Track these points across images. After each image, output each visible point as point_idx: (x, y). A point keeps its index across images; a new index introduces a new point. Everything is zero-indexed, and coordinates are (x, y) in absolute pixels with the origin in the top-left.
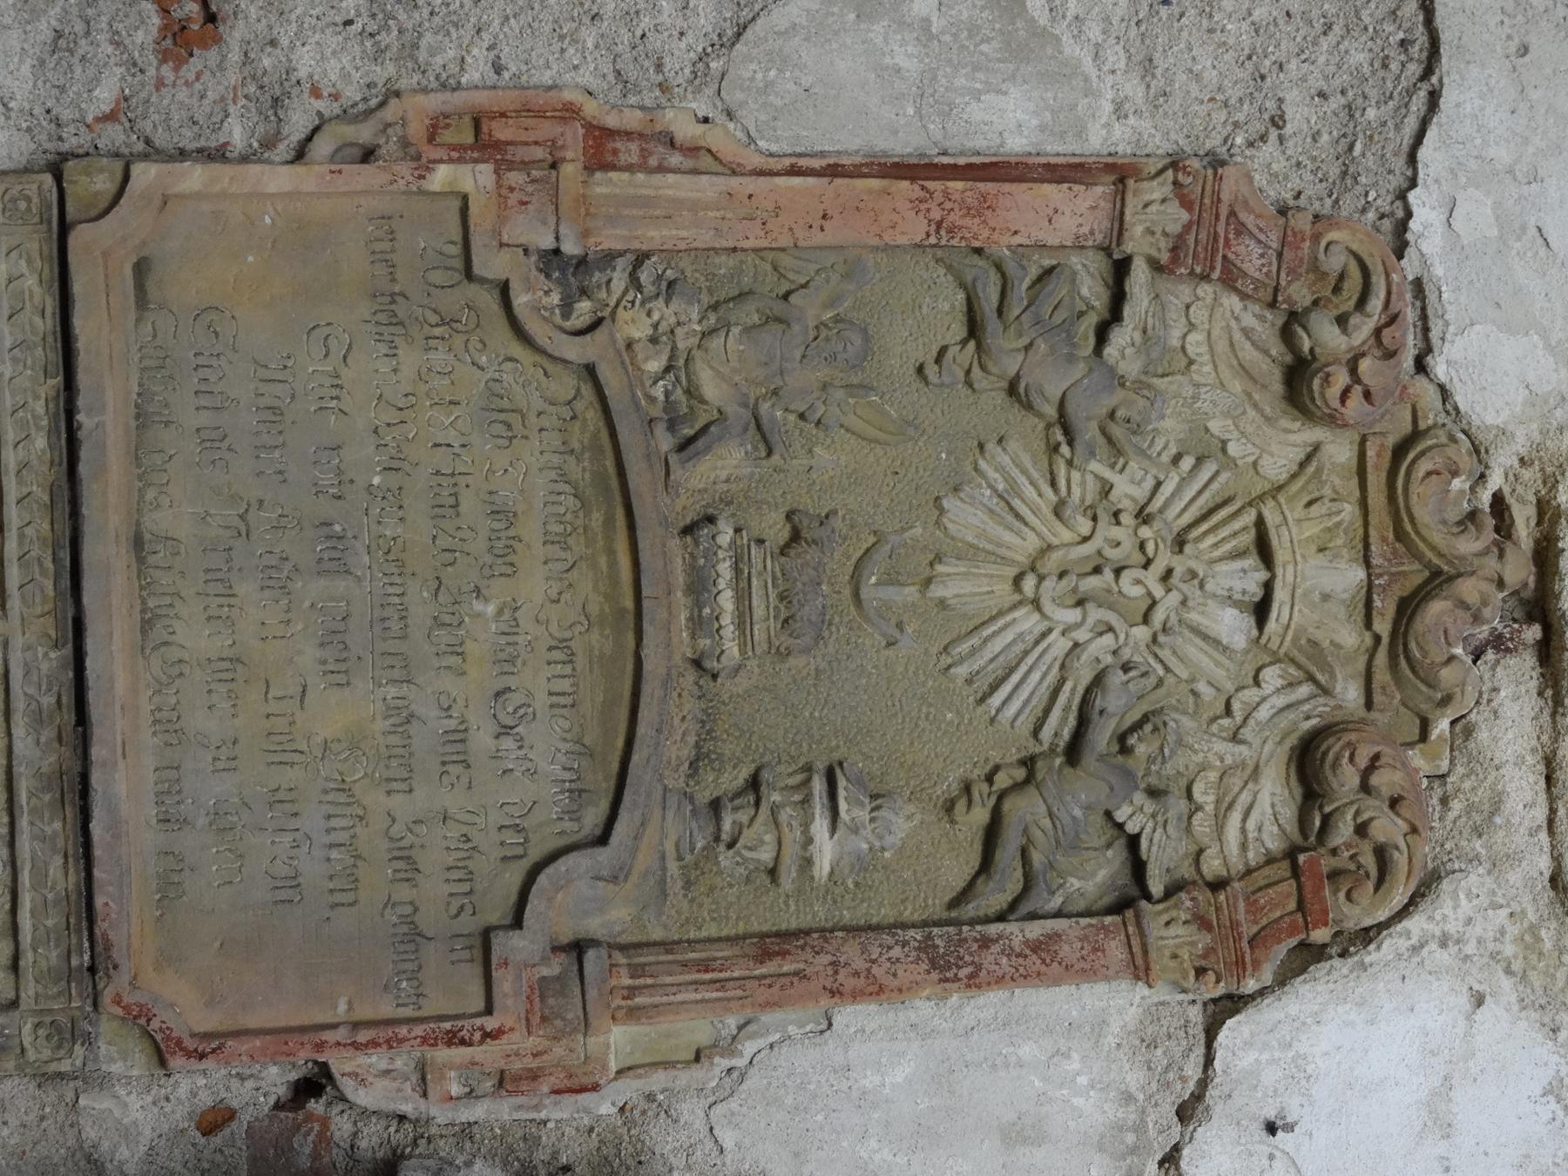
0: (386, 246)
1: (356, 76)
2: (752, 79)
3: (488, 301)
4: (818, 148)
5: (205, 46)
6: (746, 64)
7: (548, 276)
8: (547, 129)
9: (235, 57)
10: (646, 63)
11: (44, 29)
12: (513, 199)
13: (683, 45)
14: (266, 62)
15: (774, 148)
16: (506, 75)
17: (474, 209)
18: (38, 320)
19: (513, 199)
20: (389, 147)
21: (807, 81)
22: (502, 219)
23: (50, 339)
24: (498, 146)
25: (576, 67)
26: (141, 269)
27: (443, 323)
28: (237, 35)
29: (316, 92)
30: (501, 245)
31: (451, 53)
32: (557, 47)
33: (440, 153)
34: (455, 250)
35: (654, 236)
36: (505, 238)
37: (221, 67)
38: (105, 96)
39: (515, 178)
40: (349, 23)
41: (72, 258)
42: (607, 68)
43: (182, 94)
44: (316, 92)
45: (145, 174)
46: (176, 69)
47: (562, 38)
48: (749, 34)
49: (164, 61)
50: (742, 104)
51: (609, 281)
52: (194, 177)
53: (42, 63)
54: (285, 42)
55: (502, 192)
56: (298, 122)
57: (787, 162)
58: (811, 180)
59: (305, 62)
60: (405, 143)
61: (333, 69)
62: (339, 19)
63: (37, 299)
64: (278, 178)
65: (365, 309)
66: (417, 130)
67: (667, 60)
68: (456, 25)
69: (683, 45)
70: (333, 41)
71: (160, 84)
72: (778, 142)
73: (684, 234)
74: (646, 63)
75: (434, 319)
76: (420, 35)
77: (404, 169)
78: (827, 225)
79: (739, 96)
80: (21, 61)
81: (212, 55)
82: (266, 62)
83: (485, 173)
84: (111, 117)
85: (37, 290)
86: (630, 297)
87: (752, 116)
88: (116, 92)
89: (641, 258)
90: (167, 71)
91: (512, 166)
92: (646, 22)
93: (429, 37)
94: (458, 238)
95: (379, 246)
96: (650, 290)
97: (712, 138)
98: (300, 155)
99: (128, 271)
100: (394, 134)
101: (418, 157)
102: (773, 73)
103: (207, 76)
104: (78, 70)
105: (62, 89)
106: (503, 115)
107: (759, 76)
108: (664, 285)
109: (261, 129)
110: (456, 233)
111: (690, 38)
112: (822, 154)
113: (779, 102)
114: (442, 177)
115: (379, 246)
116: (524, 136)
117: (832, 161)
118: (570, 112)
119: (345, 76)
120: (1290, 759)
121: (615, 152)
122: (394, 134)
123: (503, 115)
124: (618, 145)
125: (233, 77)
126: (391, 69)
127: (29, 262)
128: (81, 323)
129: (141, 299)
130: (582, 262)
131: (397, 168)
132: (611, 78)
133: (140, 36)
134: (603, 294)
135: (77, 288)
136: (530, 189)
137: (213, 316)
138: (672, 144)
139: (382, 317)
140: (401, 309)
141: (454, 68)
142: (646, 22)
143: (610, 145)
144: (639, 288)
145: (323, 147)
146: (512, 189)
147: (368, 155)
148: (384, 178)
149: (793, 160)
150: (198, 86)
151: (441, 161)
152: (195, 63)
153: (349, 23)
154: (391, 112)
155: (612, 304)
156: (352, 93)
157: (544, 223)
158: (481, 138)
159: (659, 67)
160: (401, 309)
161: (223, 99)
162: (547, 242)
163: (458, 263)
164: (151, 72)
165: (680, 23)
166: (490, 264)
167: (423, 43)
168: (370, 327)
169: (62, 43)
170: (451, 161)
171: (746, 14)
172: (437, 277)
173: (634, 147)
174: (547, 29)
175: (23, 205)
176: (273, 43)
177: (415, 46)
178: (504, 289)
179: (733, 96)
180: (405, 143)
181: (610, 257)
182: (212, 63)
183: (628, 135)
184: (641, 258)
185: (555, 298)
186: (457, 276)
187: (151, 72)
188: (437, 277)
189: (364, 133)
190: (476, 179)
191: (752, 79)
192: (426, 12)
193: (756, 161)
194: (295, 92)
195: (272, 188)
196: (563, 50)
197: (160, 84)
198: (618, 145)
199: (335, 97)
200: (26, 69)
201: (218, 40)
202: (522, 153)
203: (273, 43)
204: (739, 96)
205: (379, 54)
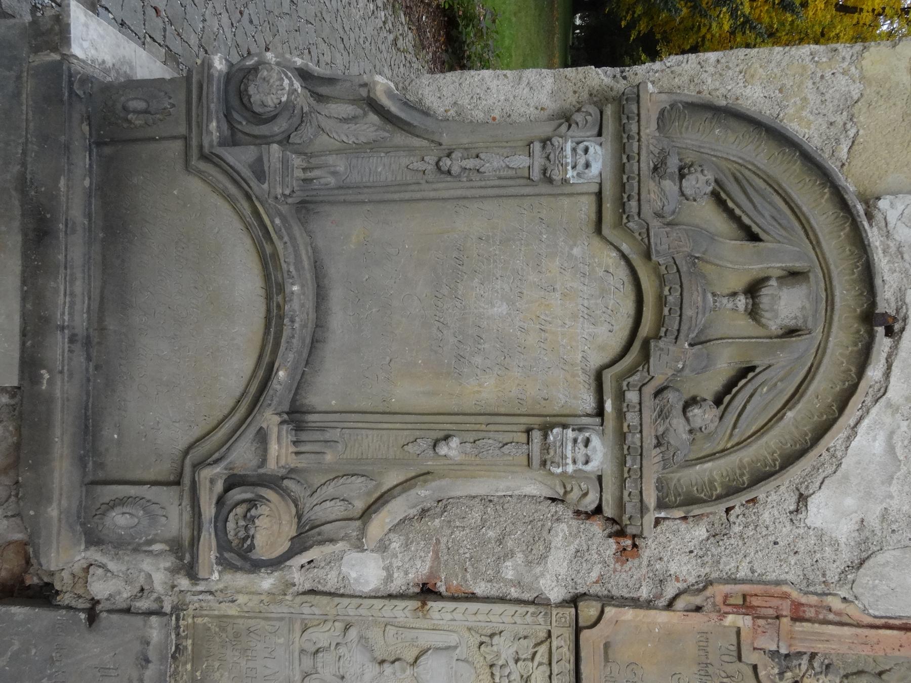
0: (705, 644)
1: (693, 573)
2: (867, 584)
3: (749, 672)
4: (897, 614)
5: (633, 558)
6: (865, 577)
7: (773, 660)
8: (775, 602)
9: (645, 563)
10: (818, 573)
11: (572, 549)
12: (760, 630)
13: (835, 566)
14: (658, 566)
15: (877, 613)
16: (756, 574)
17: (743, 634)
18: (567, 665)
19: (760, 630)
20: (708, 607)
21: (893, 585)
22: (754, 638)
23: (572, 672)
24: (753, 607)
25: (787, 573)
26: (607, 646)
27: (728, 677)
28: (646, 554)
29: (677, 579)
30: (755, 649)
31: (733, 565)
32: (778, 564)
33: (728, 609)
34: (734, 648)
35: (820, 647)
36: (756, 646)
37: (639, 566)
38: (594, 575)
39: (761, 622)
40: (691, 552)
41: (581, 643)
42: (801, 573)
43: (624, 575)
44: (677, 579)
45: (610, 611)
46: (622, 565)
47: (781, 561)
48: (866, 565)
49: (617, 562)
50: (862, 594)
51: (800, 665)
52: (629, 614)
53: (571, 562)
54: (665, 559)
55: (755, 628)
56: (670, 591)
57: (883, 621)
58: (895, 632)
59: (673, 568)
60: (714, 604)
61: (685, 569)
62: (687, 550)
63: (567, 656)
64: (662, 617)
65: (695, 669)
66: (719, 599)
67: (827, 572)
68: (735, 553)
69: (835, 566)
70: (685, 559)
71: (615, 571)
72: (881, 609)
73: (834, 647)
74: (818, 573)
75: (723, 675)
76: (721, 558)
77: (714, 616)
78: (901, 649)
79: (861, 590)
80: (564, 561)
81: (636, 561)
82: (658, 566)
83: (748, 619)
84: (597, 582)
85: (568, 653)
86: (809, 673)
87: (866, 599)
88: (598, 573)
89: (813, 656)
90: (618, 566)
91: (758, 618)
92: (818, 556)
93: (724, 559)
94: (735, 643)
95: (701, 644)
96: (818, 670)
97: (851, 610)
98: (670, 605)
99: (602, 647)
100: (710, 601)
101: (719, 611)
102: (877, 582)
103: (633, 569)
104: (584, 565)
105: (578, 572)
106: (756, 595)
107: (870, 582)
108: (824, 667)
109: (654, 591)
110: (734, 641)
111: (838, 563)
112: (900, 618)
113: (879, 594)
114: (730, 619)
115: (701, 644)
116: (764, 604)
117: (904, 621)
118: (785, 596)
119: (689, 573)
120: (869, 246)
121: (804, 612)
122: (710, 601)
123: (756, 595)
124: (805, 609)
125: (644, 571)
126: (708, 570)
127: (565, 641)
128: (583, 667)
129: (607, 659)
130: (787, 656)
131: (711, 615)
132: (802, 577)
133: (608, 552)
134: (797, 671)
135: (583, 654)
136: (767, 627)
137: (634, 666)
138: (830, 610)
139: (702, 673)
140: (710, 670)
141: (733, 570)
142: (818, 556)
143: (802, 609)
144: (813, 668)
145: (680, 604)
146: (759, 626)
147: (698, 609)
148: (706, 619)
149: (886, 620)
150: (630, 573)
151: (729, 613)
152: (629, 564)
153: (691, 552)
154: (710, 591)
155: (801, 675)
156: (692, 580)
157: (772, 640)
158: (745, 606)
159: (824, 575)
160: (710, 670)
161: (639, 579)
162: (774, 648)
163: (735, 654)
164: (612, 566)
165: (834, 557)
166: (750, 657)
167: (722, 561)
168: (697, 676)
169: (579, 554)
170: (733, 613)
171: (864, 555)
172: (726, 658)
173: (813, 610)
174: (775, 556)
175: (563, 620)
176: (661, 559)
177: (718, 562)
178: (755, 667)
179: (857, 590)
180: (714, 604)
181: (800, 654)
182: (636, 565)
183: (811, 606)
184: (813, 656)
185: (776, 671)
186: (735, 659)
187: (612, 566)
188: (726, 658)
189: (698, 600)
190: (744, 622)
191: (867, 584)
192: (723, 548)
193: (869, 620)
194: (669, 579)
195: (659, 620)
196: (781, 566)
197: (615, 571)
198: (805, 609)
199: (685, 581)
200: (565, 564)
201: (639, 556)
202: (763, 612)
203: (661, 559)
204: (861, 590)
205: (703, 565)
